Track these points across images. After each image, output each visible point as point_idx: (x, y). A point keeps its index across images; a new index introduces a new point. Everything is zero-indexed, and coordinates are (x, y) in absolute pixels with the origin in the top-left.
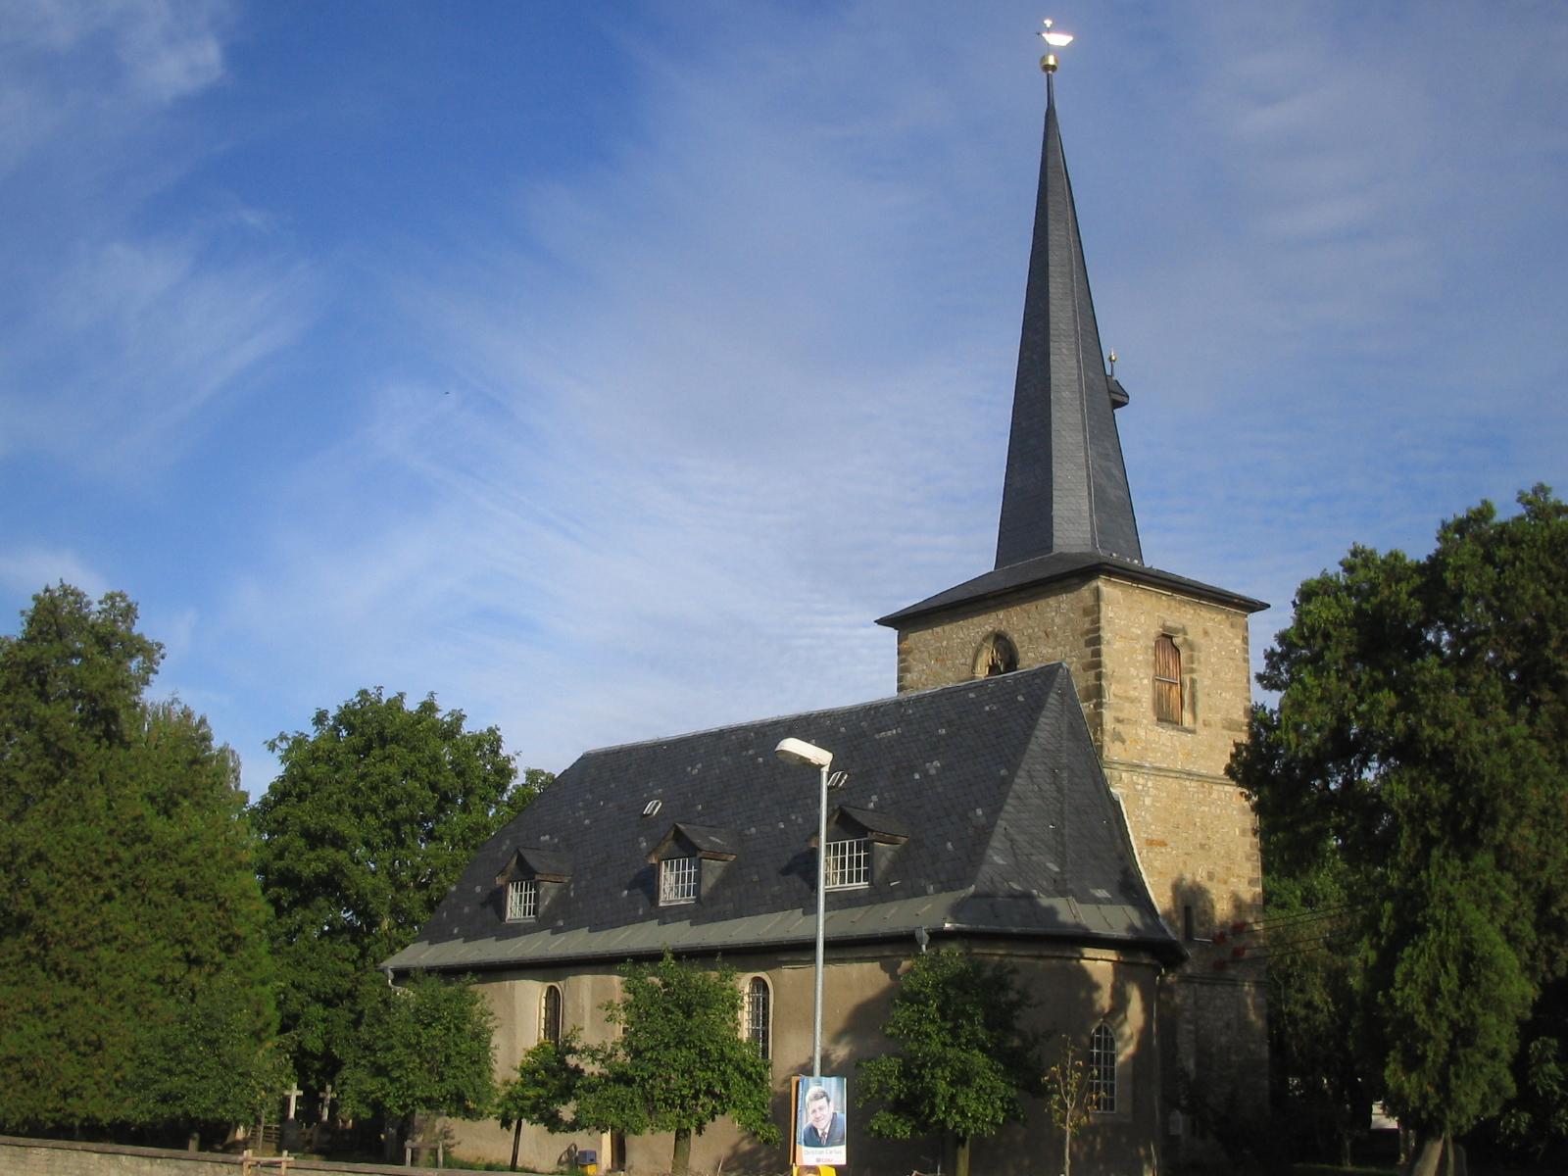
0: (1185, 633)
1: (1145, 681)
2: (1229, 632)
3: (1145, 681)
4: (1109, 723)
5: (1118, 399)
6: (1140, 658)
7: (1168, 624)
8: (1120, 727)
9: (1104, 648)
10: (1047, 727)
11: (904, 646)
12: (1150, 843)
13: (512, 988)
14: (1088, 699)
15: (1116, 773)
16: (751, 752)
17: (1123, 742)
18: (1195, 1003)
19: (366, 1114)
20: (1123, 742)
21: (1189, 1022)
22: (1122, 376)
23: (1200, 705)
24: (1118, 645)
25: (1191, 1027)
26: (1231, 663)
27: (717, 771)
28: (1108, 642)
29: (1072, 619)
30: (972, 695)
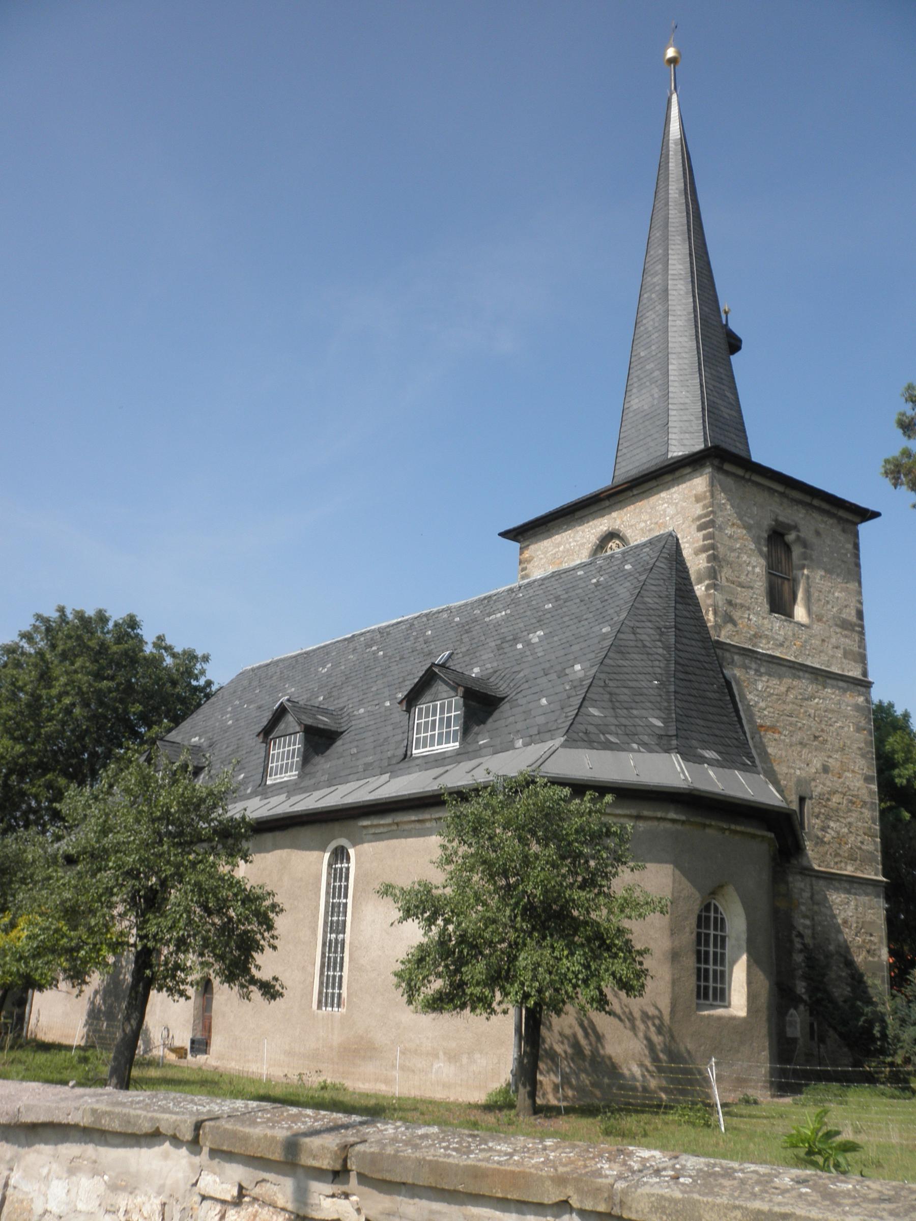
0: (799, 531)
1: (757, 570)
2: (842, 537)
3: (757, 570)
5: (734, 344)
7: (781, 519)
10: (653, 588)
15: (727, 655)
16: (374, 648)
18: (812, 898)
20: (735, 624)
21: (805, 917)
25: (808, 922)
26: (843, 566)
27: (343, 667)
29: (683, 508)
30: (580, 573)
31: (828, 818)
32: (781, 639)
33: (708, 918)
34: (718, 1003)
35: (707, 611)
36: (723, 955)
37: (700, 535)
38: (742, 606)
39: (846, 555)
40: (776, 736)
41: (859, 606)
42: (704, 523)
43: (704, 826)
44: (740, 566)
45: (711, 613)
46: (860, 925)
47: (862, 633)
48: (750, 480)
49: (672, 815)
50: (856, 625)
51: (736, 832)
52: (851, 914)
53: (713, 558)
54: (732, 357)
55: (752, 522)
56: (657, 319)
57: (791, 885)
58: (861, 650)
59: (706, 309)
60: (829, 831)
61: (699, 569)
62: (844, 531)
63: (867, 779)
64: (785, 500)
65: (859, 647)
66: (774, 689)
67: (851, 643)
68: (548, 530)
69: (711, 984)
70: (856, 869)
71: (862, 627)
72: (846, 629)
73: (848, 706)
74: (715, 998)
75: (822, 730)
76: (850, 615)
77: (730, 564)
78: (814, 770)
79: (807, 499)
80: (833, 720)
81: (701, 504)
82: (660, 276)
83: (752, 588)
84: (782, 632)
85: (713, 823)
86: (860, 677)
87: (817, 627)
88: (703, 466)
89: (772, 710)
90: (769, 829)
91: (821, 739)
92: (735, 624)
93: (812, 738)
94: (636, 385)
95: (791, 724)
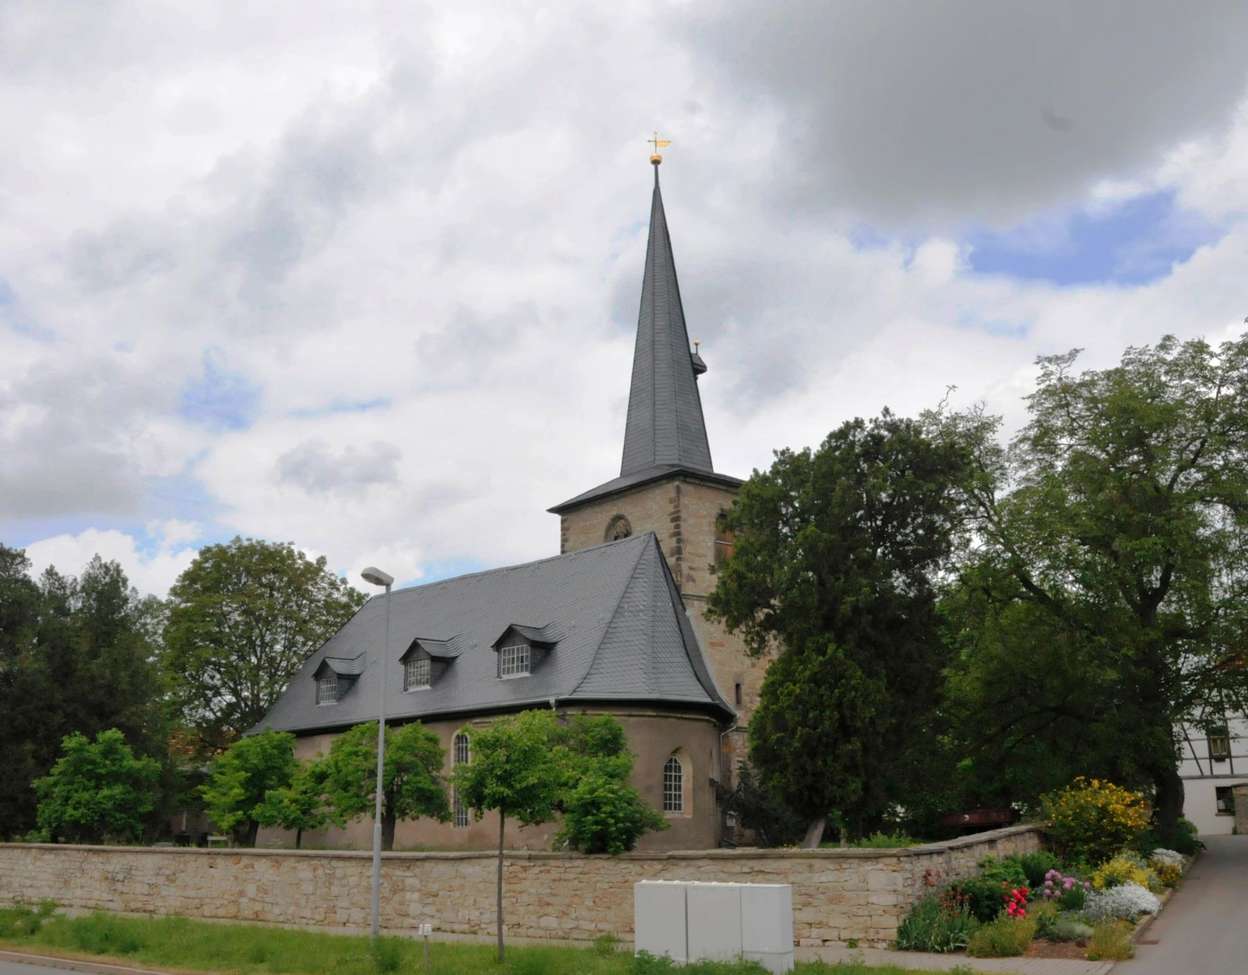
4: (685, 570)
5: (699, 369)
8: (692, 573)
9: (682, 523)
11: (566, 524)
12: (713, 644)
13: (627, 885)
14: (672, 555)
17: (694, 581)
19: (41, 793)
20: (694, 581)
24: (691, 521)
49: (649, 713)
53: (679, 541)
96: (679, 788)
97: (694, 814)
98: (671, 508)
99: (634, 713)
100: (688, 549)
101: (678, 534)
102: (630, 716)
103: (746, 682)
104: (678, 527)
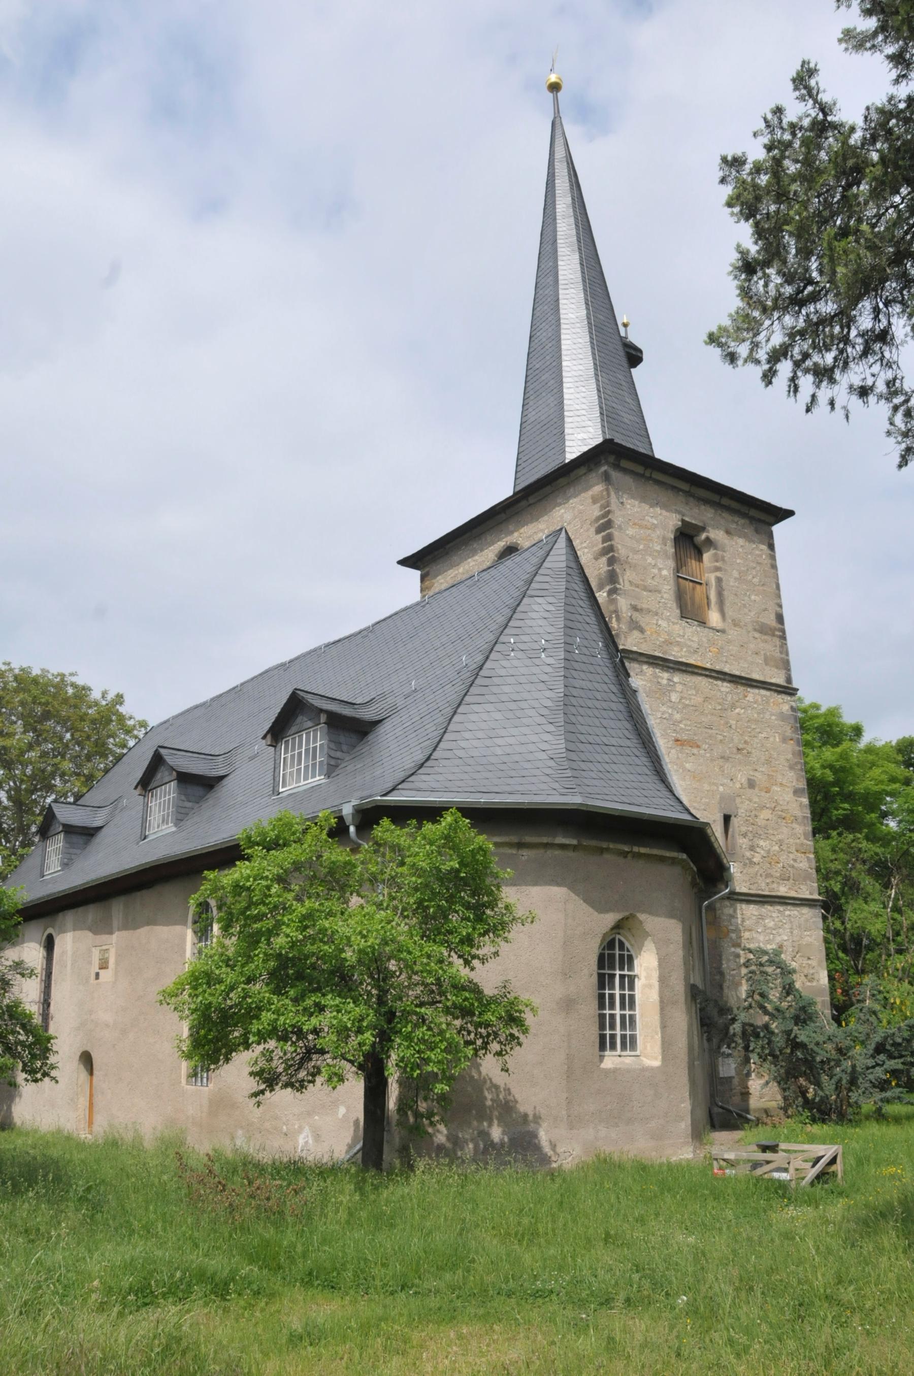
3: (665, 572)
4: (623, 603)
5: (634, 357)
6: (658, 548)
20: (642, 631)
22: (635, 338)
23: (727, 604)
26: (758, 568)
28: (620, 527)
31: (757, 835)
32: (695, 645)
33: (612, 957)
34: (628, 1053)
35: (611, 618)
36: (632, 998)
37: (599, 537)
38: (649, 611)
39: (761, 556)
40: (695, 751)
41: (778, 609)
42: (602, 524)
43: (601, 851)
44: (645, 568)
45: (614, 620)
46: (796, 949)
47: (783, 637)
48: (650, 478)
49: (560, 840)
50: (775, 629)
51: (639, 856)
52: (786, 938)
53: (611, 561)
54: (632, 370)
55: (656, 522)
56: (550, 329)
57: (718, 912)
58: (783, 656)
59: (601, 317)
60: (758, 850)
61: (600, 574)
62: (757, 531)
63: (797, 792)
64: (691, 499)
65: (781, 653)
66: (690, 699)
67: (770, 646)
68: (447, 553)
69: (618, 1032)
70: (790, 889)
71: (783, 631)
72: (766, 634)
73: (772, 715)
74: (624, 1047)
75: (746, 742)
76: (771, 621)
77: (634, 567)
78: (738, 786)
79: (716, 498)
80: (758, 730)
81: (599, 505)
82: (551, 288)
83: (660, 592)
84: (695, 639)
85: (611, 846)
86: (785, 684)
87: (733, 633)
88: (598, 464)
89: (689, 723)
90: (683, 849)
91: (745, 751)
92: (642, 631)
93: (735, 750)
94: (532, 398)
95: (710, 737)
96: (629, 1002)
97: (664, 1059)
98: (596, 511)
99: (528, 839)
100: (627, 578)
101: (611, 549)
102: (520, 845)
103: (741, 812)
104: (609, 538)
